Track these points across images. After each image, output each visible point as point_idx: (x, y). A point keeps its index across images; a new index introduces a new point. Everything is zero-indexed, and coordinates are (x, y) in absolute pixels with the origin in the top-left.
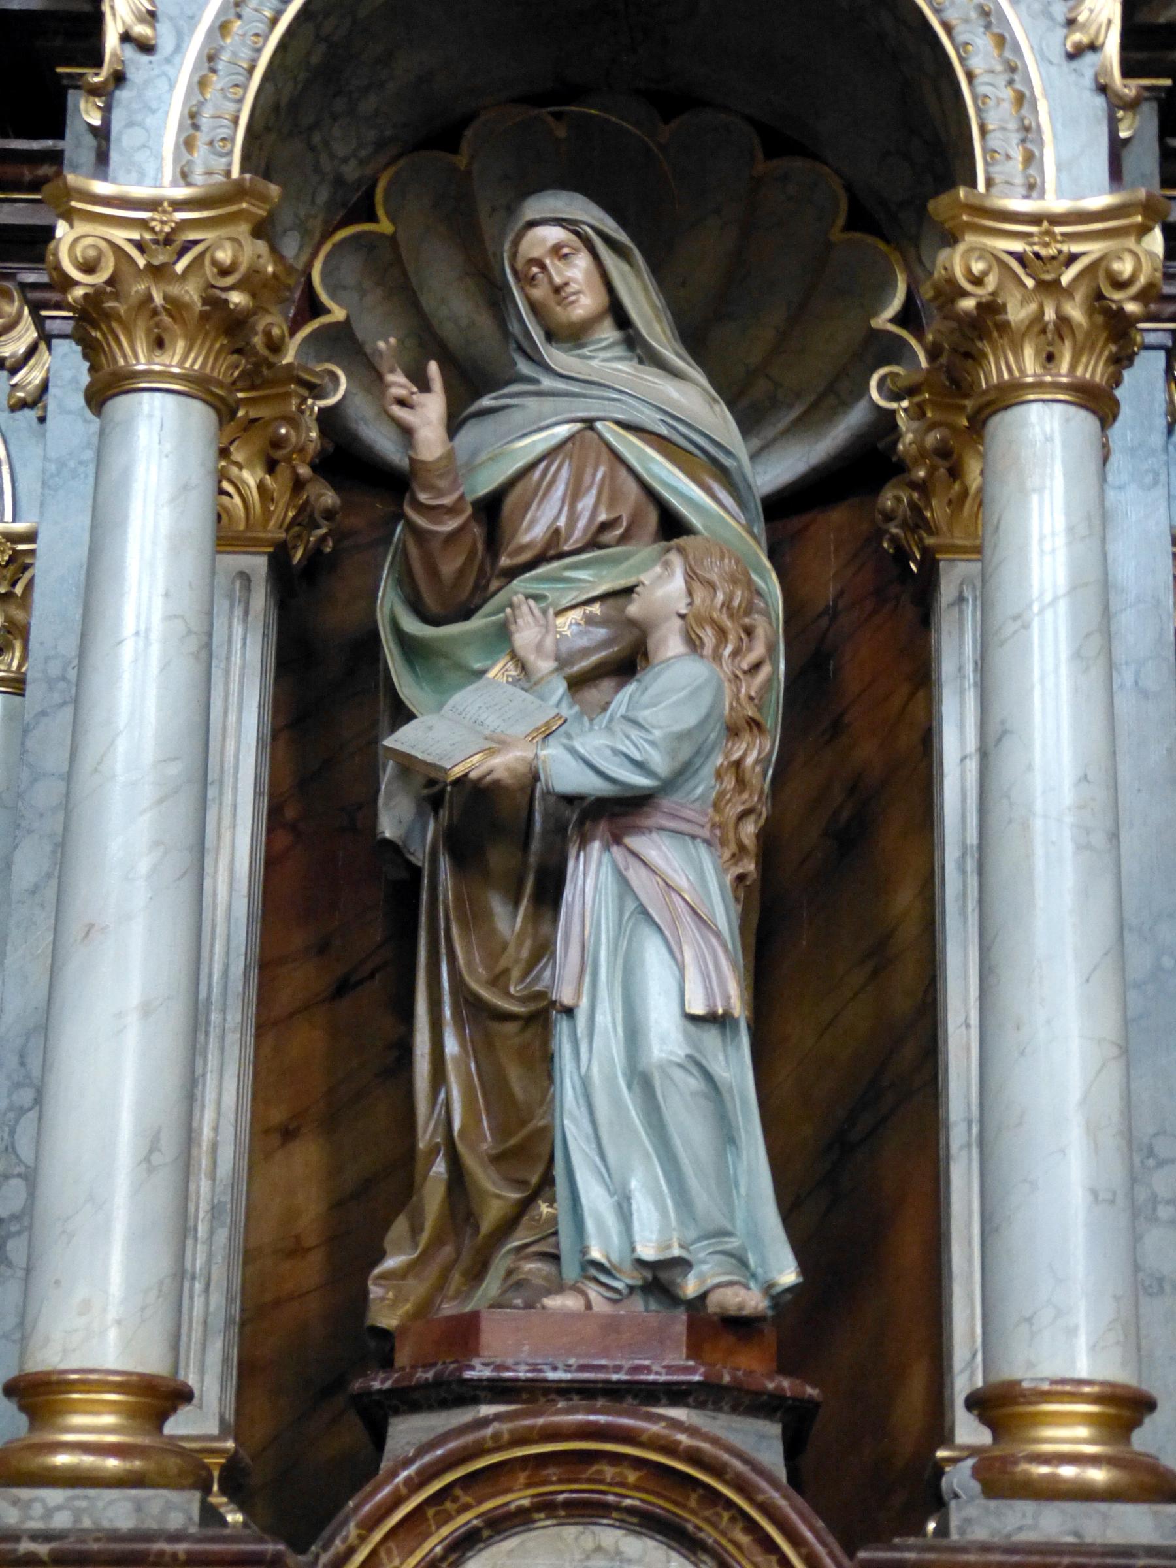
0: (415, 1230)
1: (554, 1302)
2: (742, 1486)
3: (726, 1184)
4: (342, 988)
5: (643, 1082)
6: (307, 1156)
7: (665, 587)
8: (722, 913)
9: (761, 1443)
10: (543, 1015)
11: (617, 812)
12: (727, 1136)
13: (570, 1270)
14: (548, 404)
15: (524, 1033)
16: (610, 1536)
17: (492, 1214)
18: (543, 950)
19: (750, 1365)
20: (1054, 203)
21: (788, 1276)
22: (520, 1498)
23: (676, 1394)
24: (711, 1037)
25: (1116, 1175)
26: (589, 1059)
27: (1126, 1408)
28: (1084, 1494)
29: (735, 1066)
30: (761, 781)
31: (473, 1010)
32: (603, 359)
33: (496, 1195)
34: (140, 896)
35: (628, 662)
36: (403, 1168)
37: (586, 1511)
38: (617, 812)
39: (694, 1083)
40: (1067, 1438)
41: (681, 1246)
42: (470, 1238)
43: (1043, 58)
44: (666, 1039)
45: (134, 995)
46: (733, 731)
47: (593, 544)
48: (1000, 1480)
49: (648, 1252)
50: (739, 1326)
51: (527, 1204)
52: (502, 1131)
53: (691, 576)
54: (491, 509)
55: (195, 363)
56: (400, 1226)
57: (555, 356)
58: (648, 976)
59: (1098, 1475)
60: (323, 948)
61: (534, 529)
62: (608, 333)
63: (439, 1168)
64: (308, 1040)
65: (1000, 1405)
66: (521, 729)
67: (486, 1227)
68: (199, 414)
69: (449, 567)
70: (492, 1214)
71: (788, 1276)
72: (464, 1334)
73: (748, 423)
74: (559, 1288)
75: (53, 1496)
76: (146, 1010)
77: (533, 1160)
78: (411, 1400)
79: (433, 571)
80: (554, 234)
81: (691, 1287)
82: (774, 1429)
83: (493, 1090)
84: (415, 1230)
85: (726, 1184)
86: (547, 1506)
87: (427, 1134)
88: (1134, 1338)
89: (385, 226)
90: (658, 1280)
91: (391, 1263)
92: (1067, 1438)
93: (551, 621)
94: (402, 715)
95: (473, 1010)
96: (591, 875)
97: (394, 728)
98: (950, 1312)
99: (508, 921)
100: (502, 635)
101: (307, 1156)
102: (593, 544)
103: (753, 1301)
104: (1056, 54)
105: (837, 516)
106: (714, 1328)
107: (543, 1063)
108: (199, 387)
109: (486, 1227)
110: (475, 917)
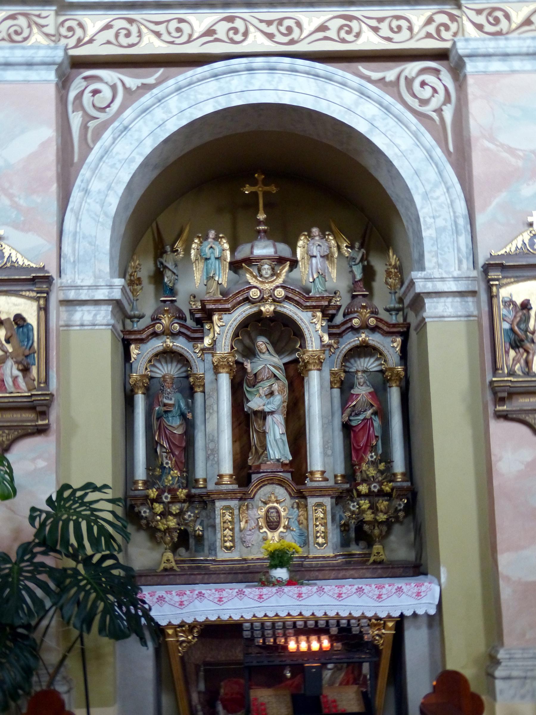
0: (252, 454)
1: (268, 463)
2: (287, 481)
3: (284, 449)
4: (240, 424)
5: (276, 441)
6: (238, 444)
7: (275, 387)
8: (283, 423)
9: (288, 476)
10: (264, 433)
11: (272, 413)
12: (284, 445)
13: (269, 459)
14: (261, 362)
15: (263, 435)
16: (274, 486)
17: (260, 453)
18: (264, 425)
19: (287, 468)
20: (314, 349)
21: (291, 459)
22: (266, 483)
23: (280, 472)
24: (282, 435)
25: (322, 450)
26: (270, 438)
27: (323, 472)
28: (319, 481)
29: (285, 438)
30: (286, 407)
31: (257, 432)
32: (266, 356)
33: (260, 450)
34: (226, 427)
35: (272, 394)
36: (250, 448)
37: (273, 483)
38: (272, 413)
39: (281, 440)
40: (318, 476)
41: (221, 294)
42: (258, 456)
43: (313, 332)
44: (278, 437)
45: (226, 437)
46: (283, 403)
47: (267, 379)
48: (312, 480)
49: (277, 458)
50: (286, 464)
51: (264, 452)
52: (260, 443)
53: (278, 386)
54: (255, 375)
55: (227, 370)
56: (250, 454)
57: (262, 356)
58: (276, 430)
59: (320, 479)
60: (238, 420)
61: (260, 378)
62: (267, 352)
63: (254, 448)
64: (237, 430)
65: (312, 473)
66: (261, 404)
67: (260, 454)
68: (228, 375)
69: (251, 382)
70: (260, 453)
71: (291, 459)
72: (259, 467)
73: (233, 23)
74: (268, 461)
75: (224, 486)
76: (228, 439)
77: (264, 447)
78: (254, 473)
79: (250, 382)
80: (261, 343)
81: (281, 461)
82: (290, 474)
83: (259, 438)
84: (252, 454)
85: (284, 449)
86: (269, 483)
87: (252, 444)
88: (325, 467)
89: (240, 338)
90: (278, 460)
91: (250, 458)
92: (318, 476)
93: (264, 388)
94: (248, 401)
95: (257, 432)
96: (269, 418)
97: (247, 403)
98: (306, 51)
99: (260, 422)
100: (258, 391)
101: (238, 444)
102: (267, 379)
103: (287, 462)
104: (314, 331)
105: (293, 365)
106: (283, 465)
107: (265, 437)
108: (227, 372)
109: (260, 454)
110: (257, 422)
